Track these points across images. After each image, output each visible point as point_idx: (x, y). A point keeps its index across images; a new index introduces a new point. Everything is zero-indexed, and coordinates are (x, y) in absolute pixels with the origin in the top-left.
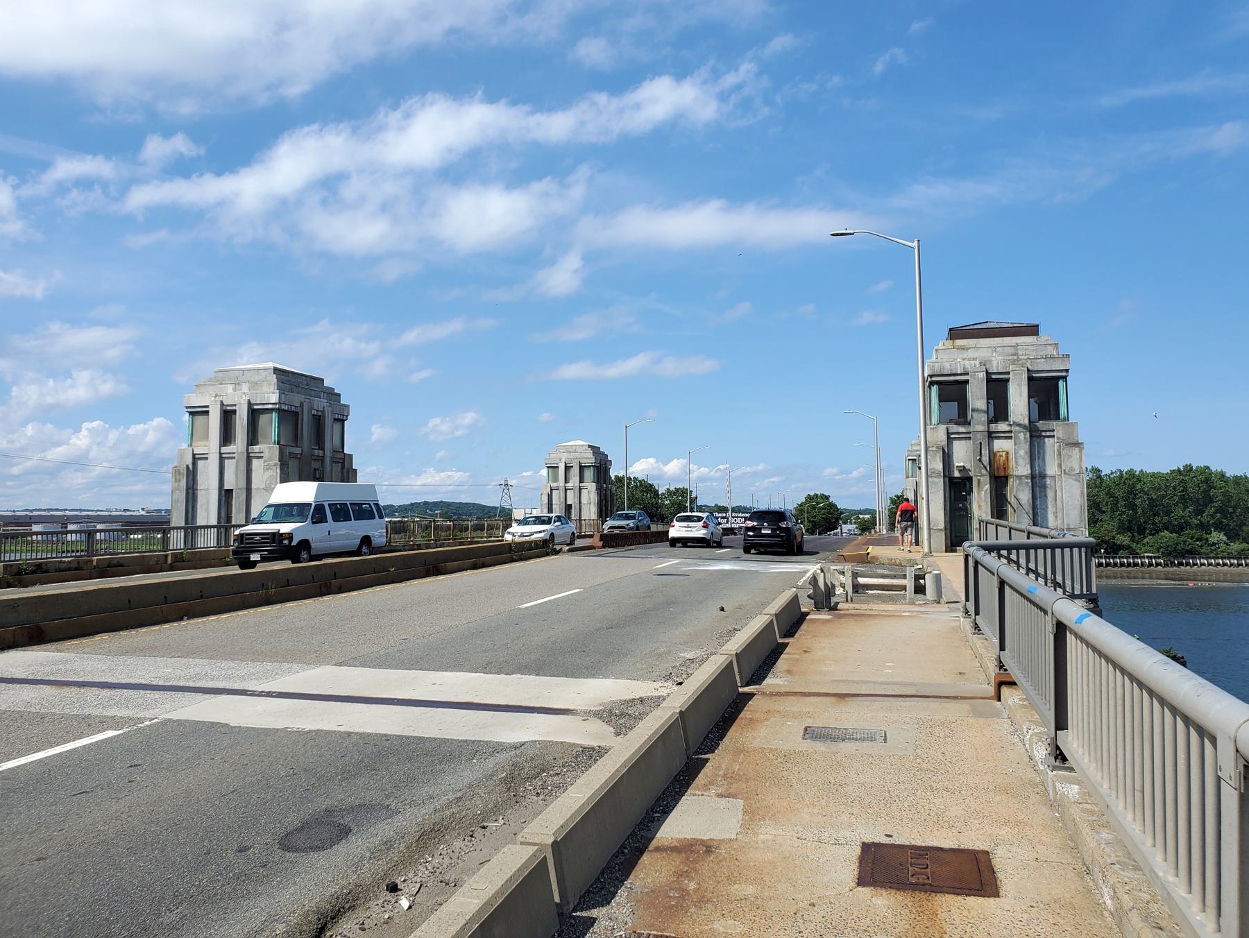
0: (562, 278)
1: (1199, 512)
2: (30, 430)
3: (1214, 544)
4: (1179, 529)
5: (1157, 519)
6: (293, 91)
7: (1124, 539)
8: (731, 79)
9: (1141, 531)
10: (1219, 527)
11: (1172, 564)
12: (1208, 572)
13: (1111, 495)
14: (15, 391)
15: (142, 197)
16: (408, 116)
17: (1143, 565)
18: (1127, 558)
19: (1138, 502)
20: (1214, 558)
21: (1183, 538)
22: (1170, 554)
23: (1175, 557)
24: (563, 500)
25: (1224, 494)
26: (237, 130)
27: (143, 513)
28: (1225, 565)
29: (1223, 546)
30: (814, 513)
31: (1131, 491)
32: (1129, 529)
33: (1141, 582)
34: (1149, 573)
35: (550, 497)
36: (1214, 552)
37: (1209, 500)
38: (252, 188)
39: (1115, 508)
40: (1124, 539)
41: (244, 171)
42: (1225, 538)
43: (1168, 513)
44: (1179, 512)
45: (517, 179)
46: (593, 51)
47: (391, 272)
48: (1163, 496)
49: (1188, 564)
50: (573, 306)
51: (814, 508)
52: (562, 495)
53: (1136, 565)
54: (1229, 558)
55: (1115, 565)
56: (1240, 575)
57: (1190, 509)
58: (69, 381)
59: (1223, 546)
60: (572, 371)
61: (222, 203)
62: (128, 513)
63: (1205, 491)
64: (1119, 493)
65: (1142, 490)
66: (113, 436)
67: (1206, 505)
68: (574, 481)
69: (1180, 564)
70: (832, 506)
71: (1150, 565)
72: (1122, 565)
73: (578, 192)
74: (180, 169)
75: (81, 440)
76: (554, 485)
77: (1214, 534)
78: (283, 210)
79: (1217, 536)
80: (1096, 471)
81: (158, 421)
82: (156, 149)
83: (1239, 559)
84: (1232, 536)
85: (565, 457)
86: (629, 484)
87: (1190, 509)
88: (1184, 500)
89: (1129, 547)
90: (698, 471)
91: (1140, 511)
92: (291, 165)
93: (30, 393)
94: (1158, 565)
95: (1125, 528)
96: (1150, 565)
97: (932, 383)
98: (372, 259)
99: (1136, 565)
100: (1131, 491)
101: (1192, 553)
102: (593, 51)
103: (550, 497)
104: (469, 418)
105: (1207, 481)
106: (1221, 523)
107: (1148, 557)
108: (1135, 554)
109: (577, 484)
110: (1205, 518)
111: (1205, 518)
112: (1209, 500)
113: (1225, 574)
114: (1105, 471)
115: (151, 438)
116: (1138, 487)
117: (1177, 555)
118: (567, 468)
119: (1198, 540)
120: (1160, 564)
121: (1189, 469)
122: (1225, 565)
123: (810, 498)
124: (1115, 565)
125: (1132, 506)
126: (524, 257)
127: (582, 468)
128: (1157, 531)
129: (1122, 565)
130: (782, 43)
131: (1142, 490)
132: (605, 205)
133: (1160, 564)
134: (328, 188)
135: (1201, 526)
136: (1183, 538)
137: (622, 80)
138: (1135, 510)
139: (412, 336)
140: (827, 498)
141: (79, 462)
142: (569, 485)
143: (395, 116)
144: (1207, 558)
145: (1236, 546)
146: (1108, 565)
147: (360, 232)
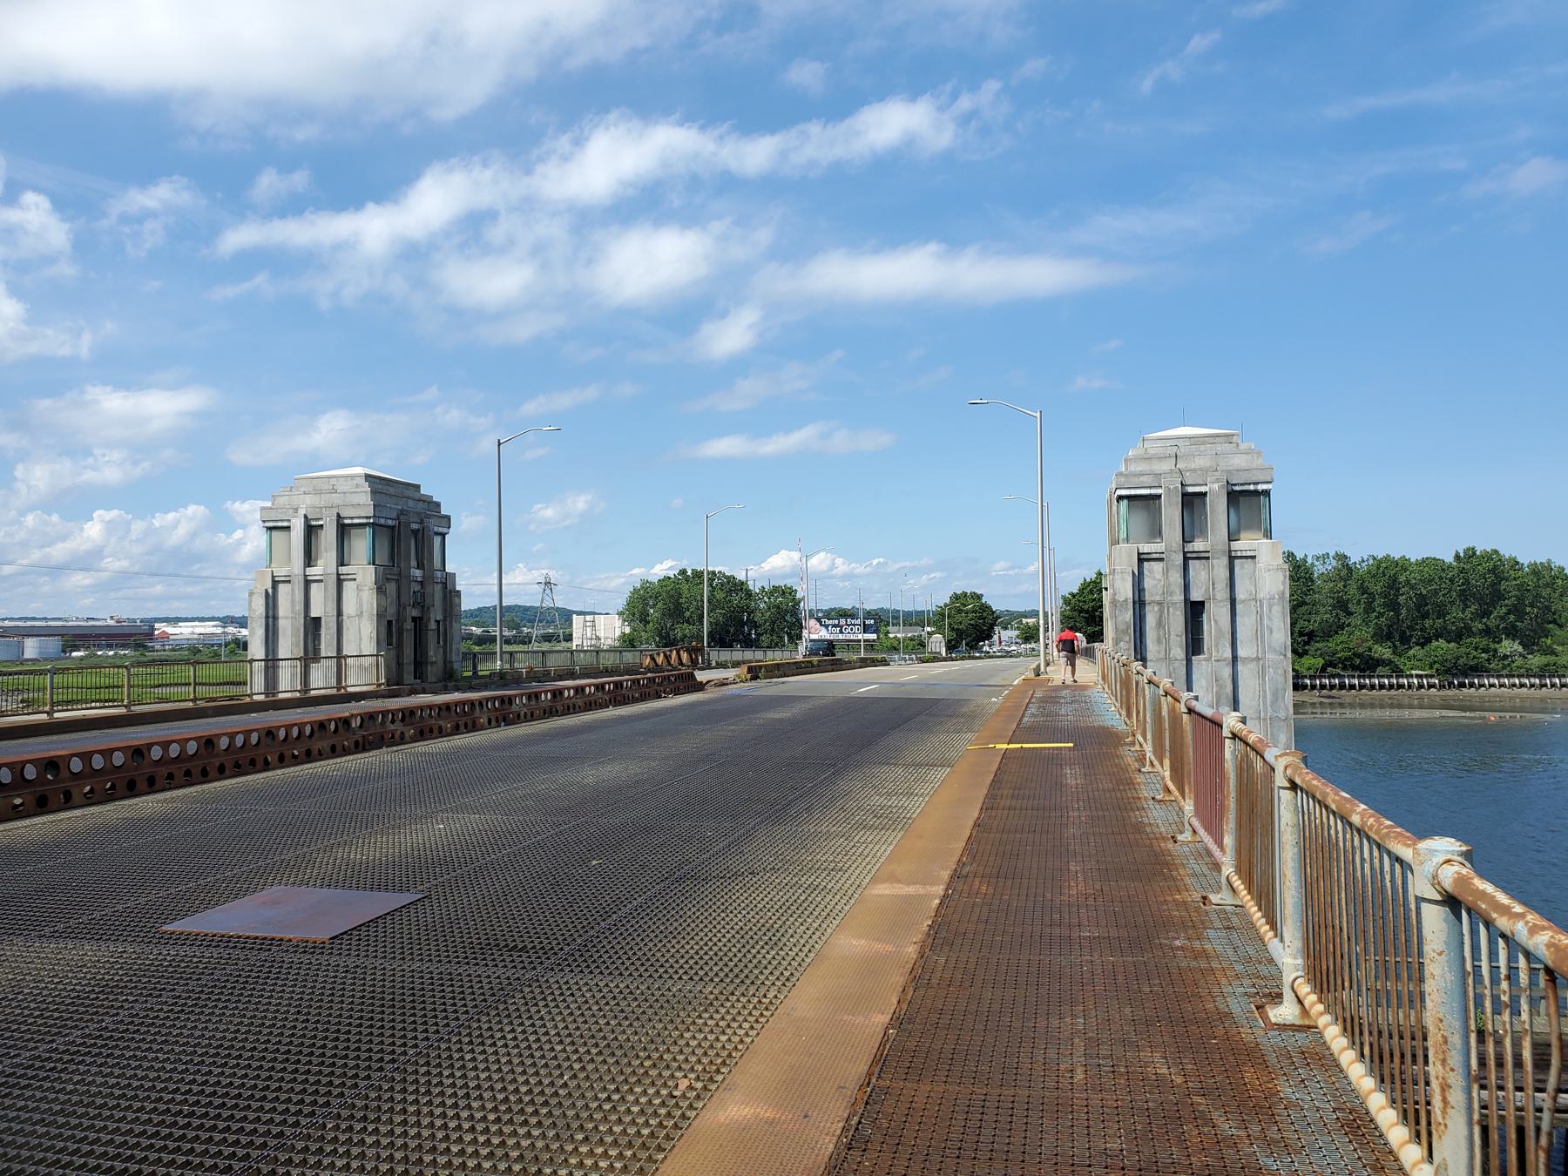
0: (731, 336)
1: (1486, 614)
2: (30, 520)
3: (1505, 657)
4: (1458, 637)
5: (1428, 623)
6: (446, 114)
7: (1383, 651)
8: (965, 103)
9: (1405, 640)
10: (1512, 633)
11: (1451, 684)
12: (1501, 696)
13: (1363, 590)
14: (19, 472)
15: (241, 237)
16: (579, 142)
17: (1410, 687)
18: (1389, 677)
19: (1402, 599)
20: (1508, 676)
21: (1463, 650)
22: (1448, 671)
23: (1455, 676)
24: (300, 607)
25: (1519, 587)
26: (358, 151)
27: (112, 623)
28: (1522, 685)
29: (1519, 661)
30: (959, 618)
31: (1393, 584)
32: (1389, 637)
33: (1406, 713)
34: (1415, 701)
35: (271, 600)
36: (1506, 668)
37: (1497, 596)
38: (374, 229)
39: (1369, 609)
40: (1383, 651)
41: (371, 207)
42: (1520, 649)
43: (1442, 614)
44: (1456, 613)
45: (688, 218)
46: (806, 75)
47: (523, 331)
48: (1436, 593)
49: (1472, 685)
50: (737, 367)
51: (960, 611)
52: (299, 596)
53: (1401, 686)
54: (1528, 677)
55: (1373, 687)
56: (1542, 700)
57: (1473, 608)
58: (90, 460)
59: (1519, 661)
60: (725, 446)
61: (339, 247)
62: (91, 623)
63: (1493, 585)
64: (1377, 588)
65: (1408, 582)
66: (138, 527)
67: (1493, 604)
68: (326, 563)
69: (1462, 685)
70: (986, 608)
71: (1421, 686)
72: (1382, 687)
73: (764, 236)
74: (292, 207)
75: (94, 530)
76: (281, 572)
77: (1505, 643)
78: (414, 255)
79: (1508, 646)
80: (1342, 558)
81: (192, 509)
82: (268, 183)
83: (1541, 677)
84: (1529, 645)
85: (306, 504)
86: (711, 580)
87: (1473, 608)
88: (1465, 597)
89: (1390, 662)
90: (818, 562)
91: (1404, 611)
92: (434, 200)
93: (38, 476)
94: (1431, 686)
95: (1382, 636)
96: (1421, 686)
97: (1120, 498)
98: (504, 314)
99: (1401, 686)
100: (1393, 584)
101: (1477, 670)
102: (806, 75)
103: (271, 600)
104: (581, 503)
105: (1494, 570)
106: (1514, 627)
107: (1418, 676)
108: (1399, 673)
109: (332, 568)
110: (1492, 622)
111: (1492, 622)
112: (1497, 596)
113: (1523, 699)
114: (1354, 558)
115: (182, 531)
116: (1402, 579)
117: (1457, 672)
118: (311, 531)
119: (1484, 651)
120: (1433, 686)
121: (1471, 553)
122: (1522, 685)
123: (956, 597)
124: (1373, 687)
125: (1394, 606)
126: (686, 313)
127: (343, 530)
128: (1428, 641)
129: (1382, 687)
130: (1034, 67)
131: (1408, 582)
132: (794, 251)
133: (1433, 686)
134: (472, 231)
135: (1487, 632)
136: (1463, 650)
137: (841, 104)
138: (1398, 614)
139: (530, 408)
140: (979, 597)
141: (86, 561)
142: (314, 572)
143: (564, 142)
144: (1498, 677)
145: (1536, 660)
146: (1362, 687)
147: (497, 282)
